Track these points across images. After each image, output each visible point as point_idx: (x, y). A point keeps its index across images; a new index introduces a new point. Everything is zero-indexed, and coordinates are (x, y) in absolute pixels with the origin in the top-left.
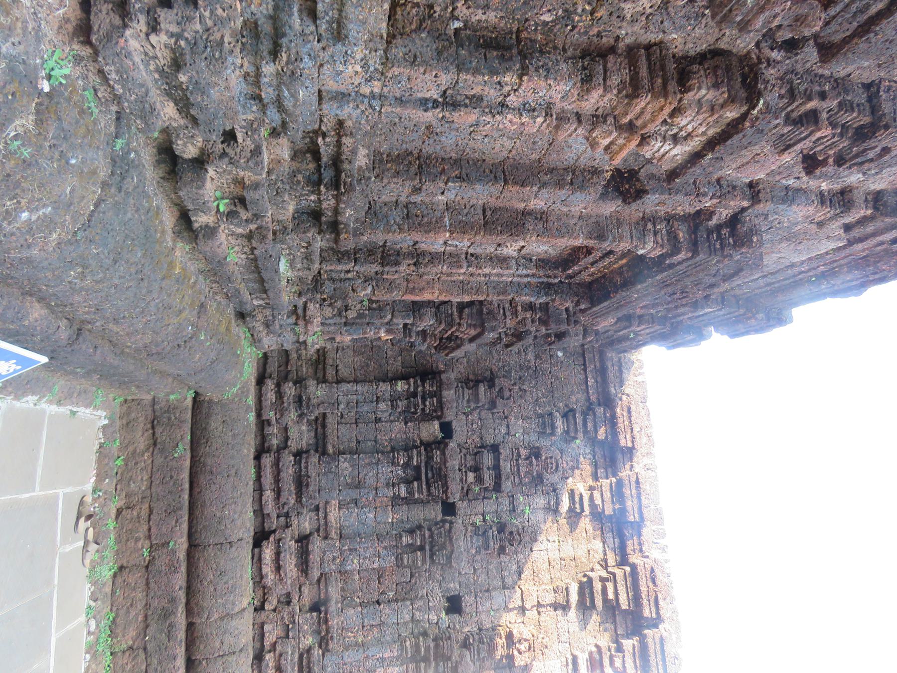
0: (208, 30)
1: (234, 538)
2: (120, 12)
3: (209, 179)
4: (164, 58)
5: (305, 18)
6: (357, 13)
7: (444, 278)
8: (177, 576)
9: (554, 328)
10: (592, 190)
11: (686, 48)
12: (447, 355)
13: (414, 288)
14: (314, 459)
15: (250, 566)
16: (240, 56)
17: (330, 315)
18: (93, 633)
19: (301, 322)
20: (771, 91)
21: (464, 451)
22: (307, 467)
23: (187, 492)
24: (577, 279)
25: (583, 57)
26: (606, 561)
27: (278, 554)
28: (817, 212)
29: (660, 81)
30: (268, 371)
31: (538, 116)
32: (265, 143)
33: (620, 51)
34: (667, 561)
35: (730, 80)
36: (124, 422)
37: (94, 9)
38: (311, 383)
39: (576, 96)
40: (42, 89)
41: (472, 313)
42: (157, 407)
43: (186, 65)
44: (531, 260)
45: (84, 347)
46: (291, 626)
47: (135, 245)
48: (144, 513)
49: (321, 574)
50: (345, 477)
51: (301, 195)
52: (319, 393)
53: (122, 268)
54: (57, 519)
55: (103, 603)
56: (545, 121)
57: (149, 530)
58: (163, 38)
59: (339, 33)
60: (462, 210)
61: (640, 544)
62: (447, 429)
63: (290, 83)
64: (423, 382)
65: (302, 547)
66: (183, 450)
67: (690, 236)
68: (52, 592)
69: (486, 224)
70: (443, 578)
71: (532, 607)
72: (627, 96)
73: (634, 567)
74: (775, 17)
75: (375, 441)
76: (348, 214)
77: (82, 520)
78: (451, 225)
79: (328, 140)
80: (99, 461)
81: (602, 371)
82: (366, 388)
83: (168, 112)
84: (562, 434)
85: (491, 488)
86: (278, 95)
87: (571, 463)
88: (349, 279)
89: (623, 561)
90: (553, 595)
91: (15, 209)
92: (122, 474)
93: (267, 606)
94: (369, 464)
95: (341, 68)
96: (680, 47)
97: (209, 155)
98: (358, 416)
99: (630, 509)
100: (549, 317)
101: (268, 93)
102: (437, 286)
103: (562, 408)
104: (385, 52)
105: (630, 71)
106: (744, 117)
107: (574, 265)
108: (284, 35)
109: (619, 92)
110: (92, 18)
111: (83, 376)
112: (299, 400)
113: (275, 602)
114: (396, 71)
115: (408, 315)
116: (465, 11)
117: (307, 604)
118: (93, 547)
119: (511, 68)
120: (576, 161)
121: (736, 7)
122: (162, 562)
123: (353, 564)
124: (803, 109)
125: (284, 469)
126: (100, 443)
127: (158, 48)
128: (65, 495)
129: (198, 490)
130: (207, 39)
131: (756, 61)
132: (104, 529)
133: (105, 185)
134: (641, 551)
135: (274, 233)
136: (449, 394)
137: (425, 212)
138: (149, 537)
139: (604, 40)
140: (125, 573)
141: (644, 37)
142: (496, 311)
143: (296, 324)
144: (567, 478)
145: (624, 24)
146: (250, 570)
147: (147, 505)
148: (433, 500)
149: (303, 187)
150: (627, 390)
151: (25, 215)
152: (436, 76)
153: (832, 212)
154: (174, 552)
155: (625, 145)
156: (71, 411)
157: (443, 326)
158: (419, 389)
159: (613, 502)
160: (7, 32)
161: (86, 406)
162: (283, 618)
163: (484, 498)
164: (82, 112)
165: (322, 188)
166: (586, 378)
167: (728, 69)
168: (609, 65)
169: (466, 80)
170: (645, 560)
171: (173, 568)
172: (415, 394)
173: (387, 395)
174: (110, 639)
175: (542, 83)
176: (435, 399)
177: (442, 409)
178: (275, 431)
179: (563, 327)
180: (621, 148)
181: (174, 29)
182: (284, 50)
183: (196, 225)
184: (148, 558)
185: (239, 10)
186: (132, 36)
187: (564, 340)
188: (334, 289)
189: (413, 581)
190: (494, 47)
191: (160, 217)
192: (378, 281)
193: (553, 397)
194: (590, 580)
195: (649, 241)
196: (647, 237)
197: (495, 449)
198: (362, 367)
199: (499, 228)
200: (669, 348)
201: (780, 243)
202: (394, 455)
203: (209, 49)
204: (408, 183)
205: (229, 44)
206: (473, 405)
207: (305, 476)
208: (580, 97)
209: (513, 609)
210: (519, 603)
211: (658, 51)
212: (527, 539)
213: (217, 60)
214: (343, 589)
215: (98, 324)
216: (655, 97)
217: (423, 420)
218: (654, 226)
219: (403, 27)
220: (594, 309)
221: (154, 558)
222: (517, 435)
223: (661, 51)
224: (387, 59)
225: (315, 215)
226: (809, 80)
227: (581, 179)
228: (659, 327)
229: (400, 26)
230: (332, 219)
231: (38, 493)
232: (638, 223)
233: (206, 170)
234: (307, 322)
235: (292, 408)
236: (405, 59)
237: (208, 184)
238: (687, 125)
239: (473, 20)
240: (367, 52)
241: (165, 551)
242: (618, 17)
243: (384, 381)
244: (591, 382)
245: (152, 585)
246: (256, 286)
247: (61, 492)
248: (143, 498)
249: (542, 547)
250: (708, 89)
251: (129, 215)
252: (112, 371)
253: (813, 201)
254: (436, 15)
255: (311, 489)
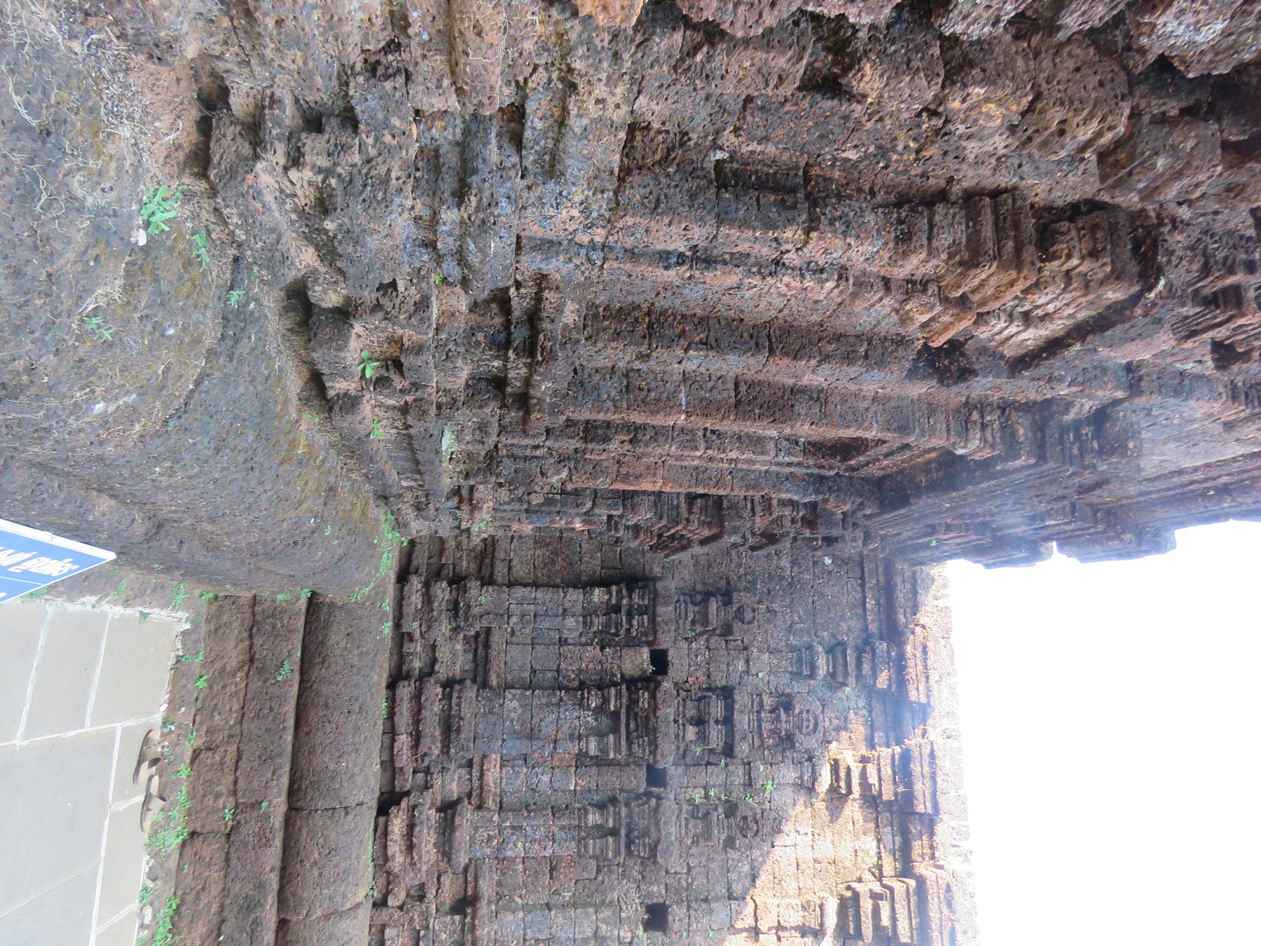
0: (369, 161)
1: (351, 802)
2: (251, 137)
3: (354, 336)
4: (306, 197)
5: (505, 145)
6: (580, 146)
7: (671, 462)
8: (269, 851)
9: (822, 531)
10: (895, 367)
11: (1052, 197)
12: (667, 556)
13: (627, 475)
14: (470, 692)
15: (371, 840)
16: (411, 196)
17: (507, 499)
18: (147, 927)
19: (465, 507)
20: (1177, 266)
21: (683, 694)
22: (459, 705)
23: (291, 731)
24: (863, 473)
25: (898, 205)
26: (880, 867)
27: (411, 827)
28: (1225, 409)
29: (1010, 244)
30: (415, 563)
31: (827, 280)
32: (435, 292)
33: (953, 198)
34: (969, 875)
35: (1115, 245)
36: (212, 626)
37: (215, 133)
38: (474, 584)
39: (886, 260)
40: (136, 243)
41: (706, 507)
42: (258, 609)
43: (335, 209)
44: (797, 443)
45: (166, 543)
46: (422, 933)
47: (246, 427)
48: (230, 759)
49: (470, 860)
50: (512, 722)
51: (480, 360)
52: (482, 599)
53: (225, 458)
54: (110, 764)
55: (166, 883)
56: (838, 286)
57: (236, 782)
58: (308, 174)
59: (552, 166)
60: (705, 382)
61: (932, 847)
62: (660, 661)
63: (479, 235)
64: (630, 591)
65: (445, 819)
66: (289, 672)
67: (1034, 433)
68: (96, 869)
69: (738, 404)
70: (644, 877)
71: (770, 929)
72: (961, 263)
73: (921, 881)
74: (1197, 185)
75: (558, 672)
76: (544, 387)
77: (146, 764)
78: (688, 403)
79: (523, 291)
80: (174, 682)
81: (888, 591)
82: (550, 595)
83: (306, 258)
84: (825, 677)
85: (720, 749)
86: (461, 246)
87: (836, 722)
88: (536, 457)
89: (906, 871)
90: (801, 913)
91: (87, 401)
92: (204, 700)
93: (391, 901)
94: (547, 705)
95: (552, 212)
96: (1043, 195)
97: (356, 307)
98: (535, 634)
99: (918, 794)
100: (817, 517)
101: (446, 244)
102: (660, 472)
103: (827, 639)
104: (616, 193)
105: (968, 227)
106: (1135, 299)
107: (859, 455)
108: (475, 171)
109: (951, 256)
110: (212, 145)
111: (162, 572)
112: (454, 607)
113: (402, 896)
114: (630, 220)
115: (616, 504)
116: (732, 138)
117: (448, 902)
118: (157, 804)
119: (794, 219)
120: (875, 326)
121: (1138, 169)
122: (248, 831)
123: (517, 848)
124: (1220, 285)
125: (428, 704)
126: (178, 656)
127: (299, 186)
128: (124, 730)
129: (306, 730)
130: (367, 174)
131: (1155, 221)
132: (173, 777)
133: (211, 354)
134: (933, 857)
135: (439, 407)
136: (665, 611)
137: (653, 384)
138: (234, 793)
139: (932, 181)
140: (198, 842)
141: (991, 180)
142: (741, 505)
143: (458, 508)
144: (829, 742)
145: (964, 166)
146: (370, 849)
147: (235, 748)
148: (635, 762)
149: (484, 350)
150: (922, 618)
151: (99, 407)
152: (685, 229)
153: (1248, 411)
154: (267, 816)
155: (951, 323)
156: (141, 612)
157: (664, 522)
158: (625, 602)
159: (895, 782)
160: (95, 179)
161: (163, 607)
162: (412, 920)
163: (708, 763)
164: (188, 263)
165: (511, 354)
166: (864, 597)
167: (1113, 229)
168: (937, 218)
169: (728, 236)
170: (939, 871)
171: (263, 840)
172: (617, 609)
173: (579, 608)
174: (170, 936)
175: (839, 242)
176: (645, 617)
177: (655, 633)
178: (419, 649)
179: (835, 532)
180: (946, 328)
181: (323, 162)
182: (474, 192)
183: (331, 393)
184: (230, 823)
185: (415, 136)
186: (265, 170)
187: (836, 546)
188: (516, 471)
189: (600, 878)
190: (771, 188)
191: (283, 381)
192: (577, 462)
193: (814, 622)
194: (856, 896)
195: (974, 438)
196: (971, 432)
197: (727, 693)
198: (545, 565)
199: (757, 411)
200: (987, 566)
201: (1165, 443)
202: (582, 694)
203: (369, 188)
204: (630, 349)
205: (398, 179)
206: (699, 629)
207: (455, 716)
208: (892, 262)
209: (742, 930)
210: (751, 922)
211: (1010, 201)
212: (767, 829)
213: (379, 203)
214: (499, 884)
215: (187, 523)
216: (1003, 267)
217: (628, 645)
218: (982, 417)
219: (643, 158)
220: (885, 516)
221: (239, 823)
222: (761, 675)
223: (1014, 201)
224: (618, 204)
225: (498, 383)
226: (1231, 244)
227: (880, 351)
228: (974, 537)
229: (638, 156)
230: (521, 391)
231: (88, 728)
232: (958, 411)
233: (352, 326)
234: (474, 508)
235: (444, 619)
236: (643, 204)
237: (353, 344)
238: (1047, 303)
239: (744, 151)
240: (590, 194)
241: (255, 814)
242: (956, 157)
243: (575, 587)
244: (870, 603)
245: (234, 862)
246: (407, 465)
247: (119, 727)
248: (230, 736)
249: (788, 841)
250: (1083, 258)
251: (241, 389)
252: (200, 569)
253: (1220, 394)
254: (692, 143)
255: (463, 736)
